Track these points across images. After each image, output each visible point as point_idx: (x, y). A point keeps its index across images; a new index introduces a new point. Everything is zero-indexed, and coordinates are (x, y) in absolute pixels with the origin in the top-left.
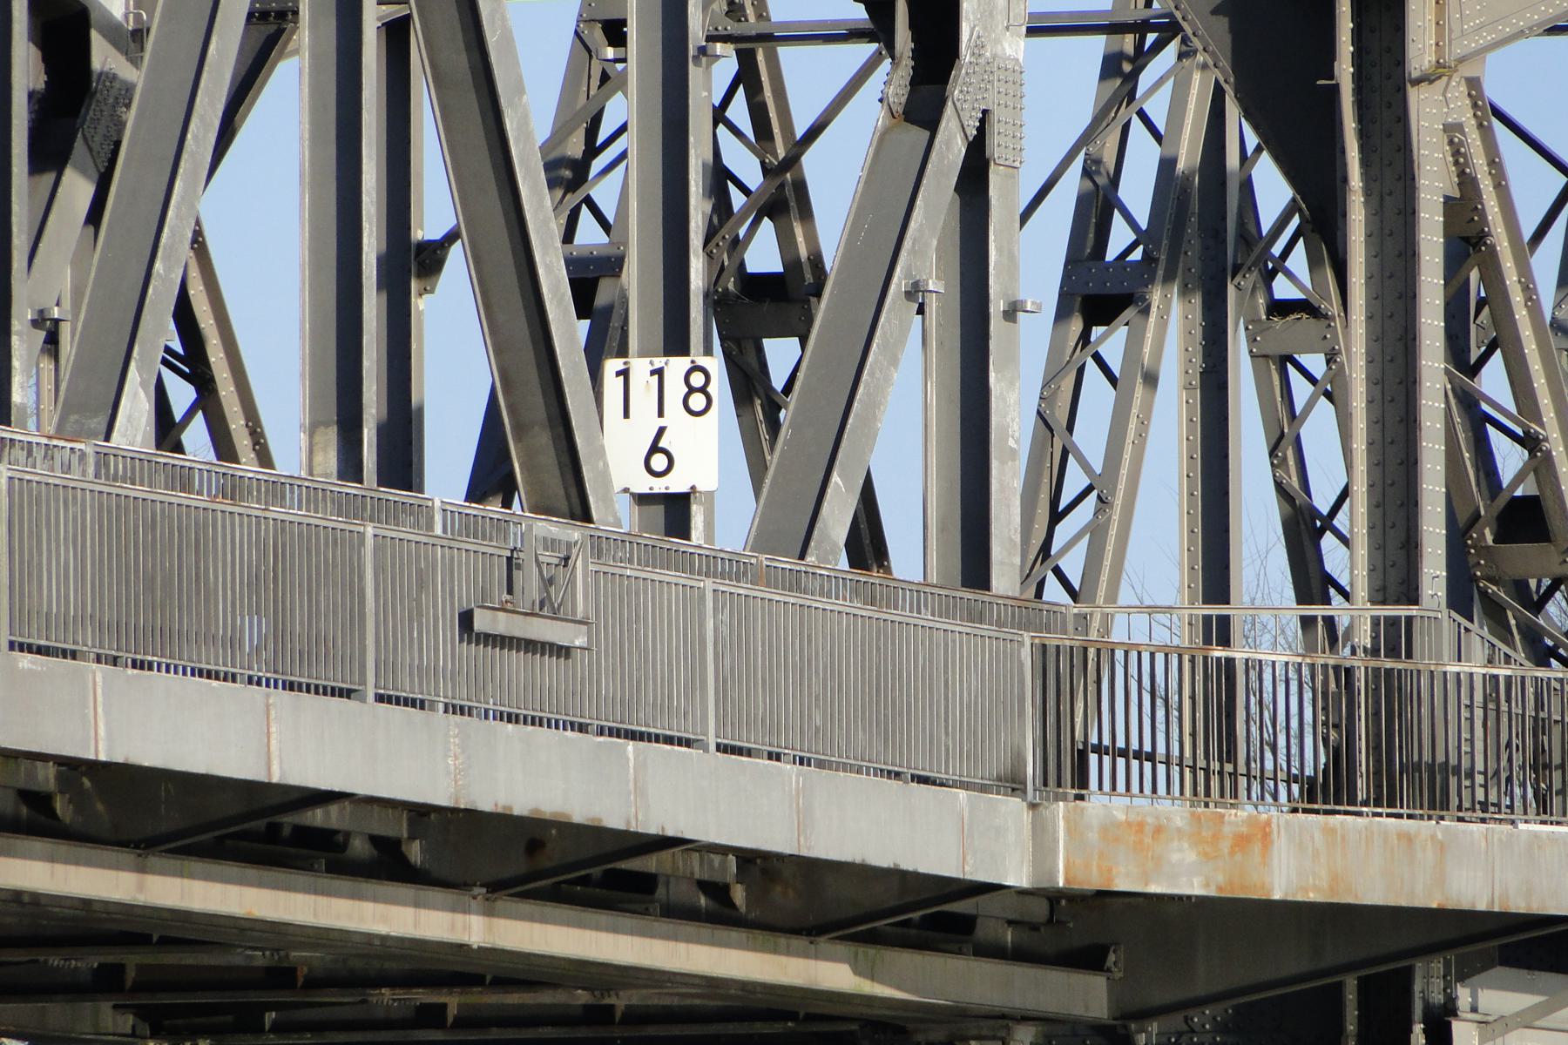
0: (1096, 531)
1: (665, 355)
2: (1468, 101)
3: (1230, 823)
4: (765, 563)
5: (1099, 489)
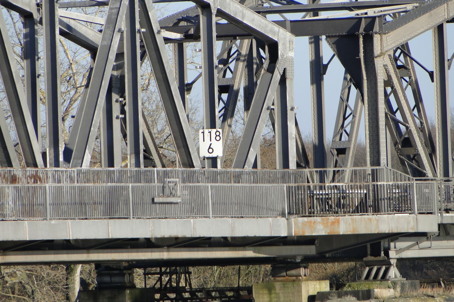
0: (353, 123)
1: (211, 129)
2: (389, 59)
3: (330, 219)
4: (233, 170)
5: (353, 114)
